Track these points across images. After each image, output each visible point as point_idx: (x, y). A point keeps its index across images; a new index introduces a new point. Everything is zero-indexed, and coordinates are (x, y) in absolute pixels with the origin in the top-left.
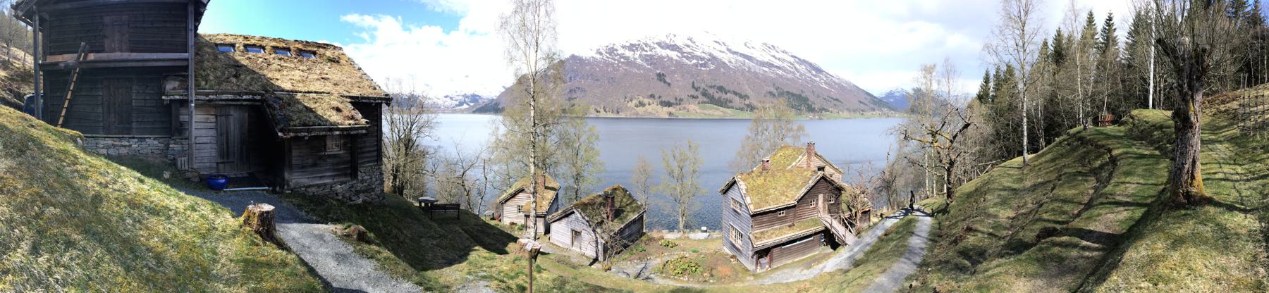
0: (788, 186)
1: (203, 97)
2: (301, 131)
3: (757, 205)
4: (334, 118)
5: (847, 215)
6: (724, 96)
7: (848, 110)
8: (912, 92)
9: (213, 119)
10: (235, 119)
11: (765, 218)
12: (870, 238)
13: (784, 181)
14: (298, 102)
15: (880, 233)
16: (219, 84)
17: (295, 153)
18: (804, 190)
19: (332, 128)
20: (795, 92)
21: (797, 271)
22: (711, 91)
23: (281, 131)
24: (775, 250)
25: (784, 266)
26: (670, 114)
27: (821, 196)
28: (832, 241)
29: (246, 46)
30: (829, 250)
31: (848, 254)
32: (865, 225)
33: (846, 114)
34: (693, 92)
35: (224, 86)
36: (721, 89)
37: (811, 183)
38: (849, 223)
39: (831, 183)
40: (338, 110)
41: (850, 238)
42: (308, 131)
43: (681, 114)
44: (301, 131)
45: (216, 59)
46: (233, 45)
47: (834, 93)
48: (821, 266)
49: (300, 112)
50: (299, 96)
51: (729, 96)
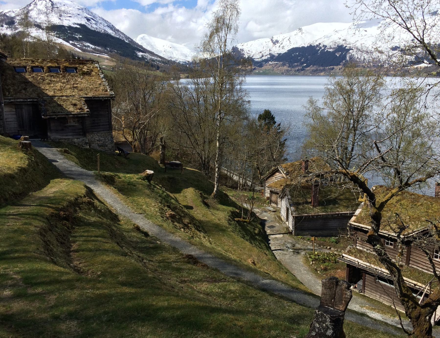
1: (8, 101)
2: (52, 115)
4: (71, 109)
9: (14, 110)
10: (26, 112)
14: (55, 102)
16: (16, 94)
17: (52, 125)
19: (69, 113)
23: (43, 115)
29: (32, 68)
35: (18, 95)
40: (75, 105)
42: (56, 115)
44: (52, 115)
45: (14, 78)
46: (25, 67)
49: (54, 107)
50: (56, 99)
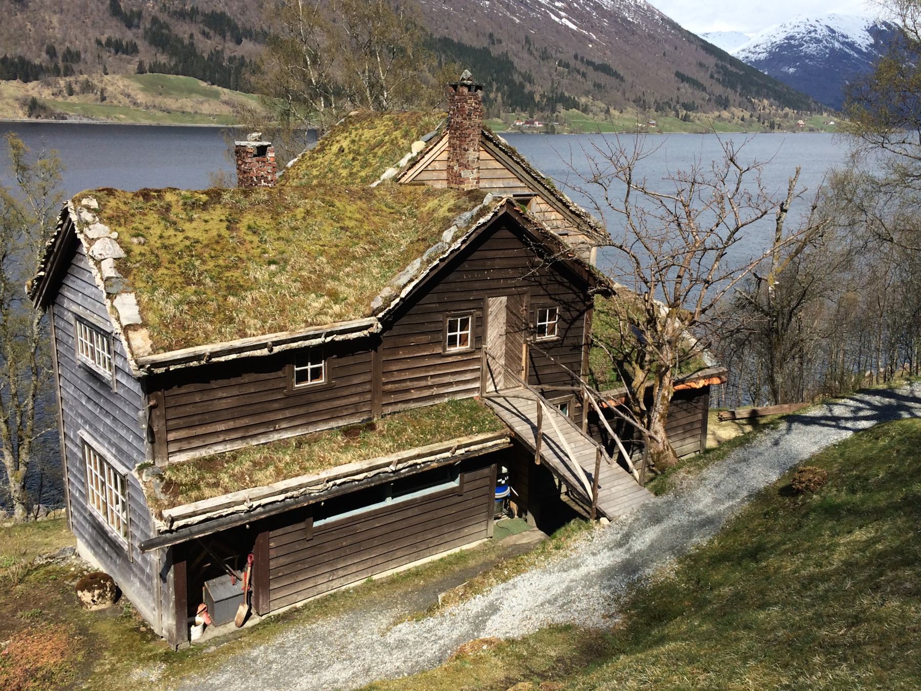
0: (344, 256)
3: (169, 331)
5: (612, 396)
6: (230, 49)
7: (641, 104)
8: (863, 40)
11: (224, 395)
12: (712, 496)
13: (327, 232)
15: (762, 475)
18: (415, 271)
20: (468, 39)
21: (372, 627)
22: (183, 30)
24: (275, 540)
25: (324, 606)
26: (33, 106)
27: (497, 306)
28: (552, 505)
30: (528, 533)
31: (607, 559)
32: (688, 447)
33: (629, 116)
34: (114, 31)
36: (218, 23)
37: (451, 240)
38: (618, 433)
39: (544, 243)
41: (620, 492)
43: (76, 110)
47: (596, 45)
48: (476, 604)
51: (248, 47)
